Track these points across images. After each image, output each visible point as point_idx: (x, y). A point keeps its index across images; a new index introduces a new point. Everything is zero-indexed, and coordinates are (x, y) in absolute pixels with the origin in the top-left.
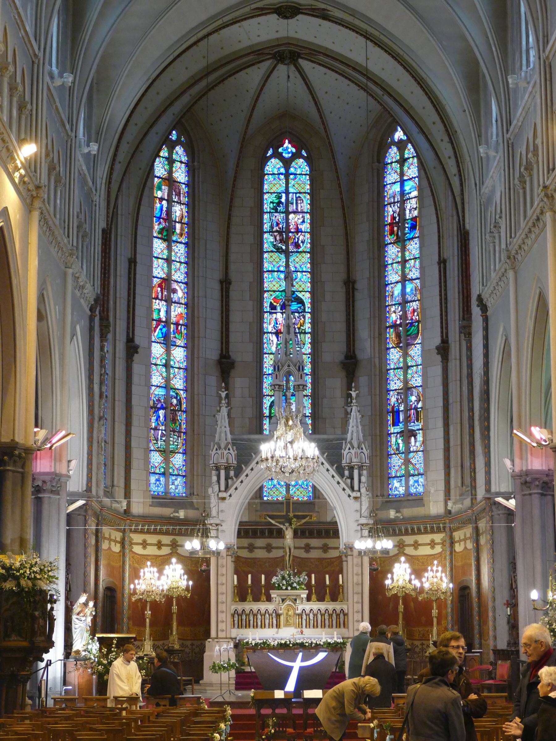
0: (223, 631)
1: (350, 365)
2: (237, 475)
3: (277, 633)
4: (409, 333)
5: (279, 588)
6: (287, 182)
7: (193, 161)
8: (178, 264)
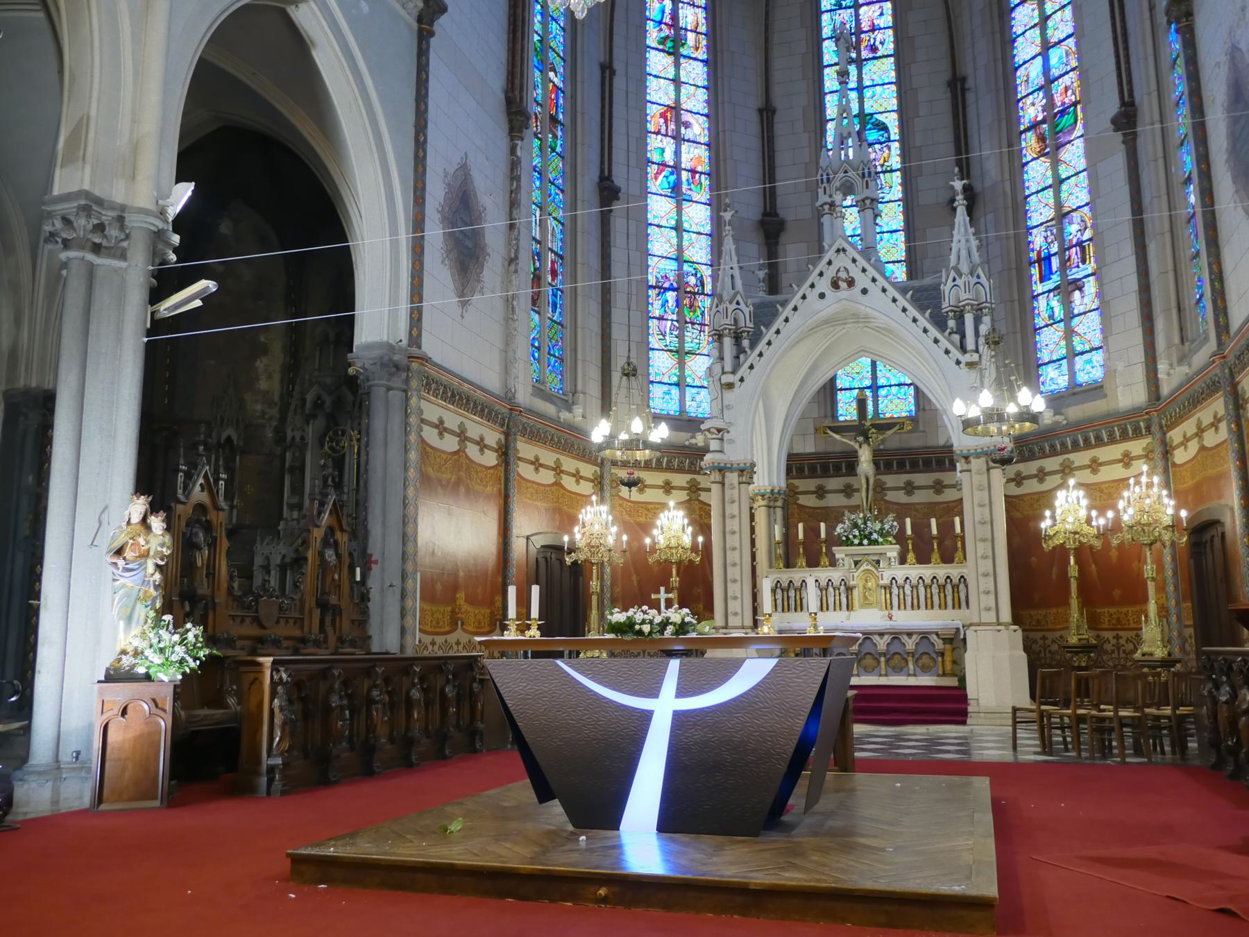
0: (736, 614)
2: (753, 346)
3: (848, 619)
5: (848, 543)
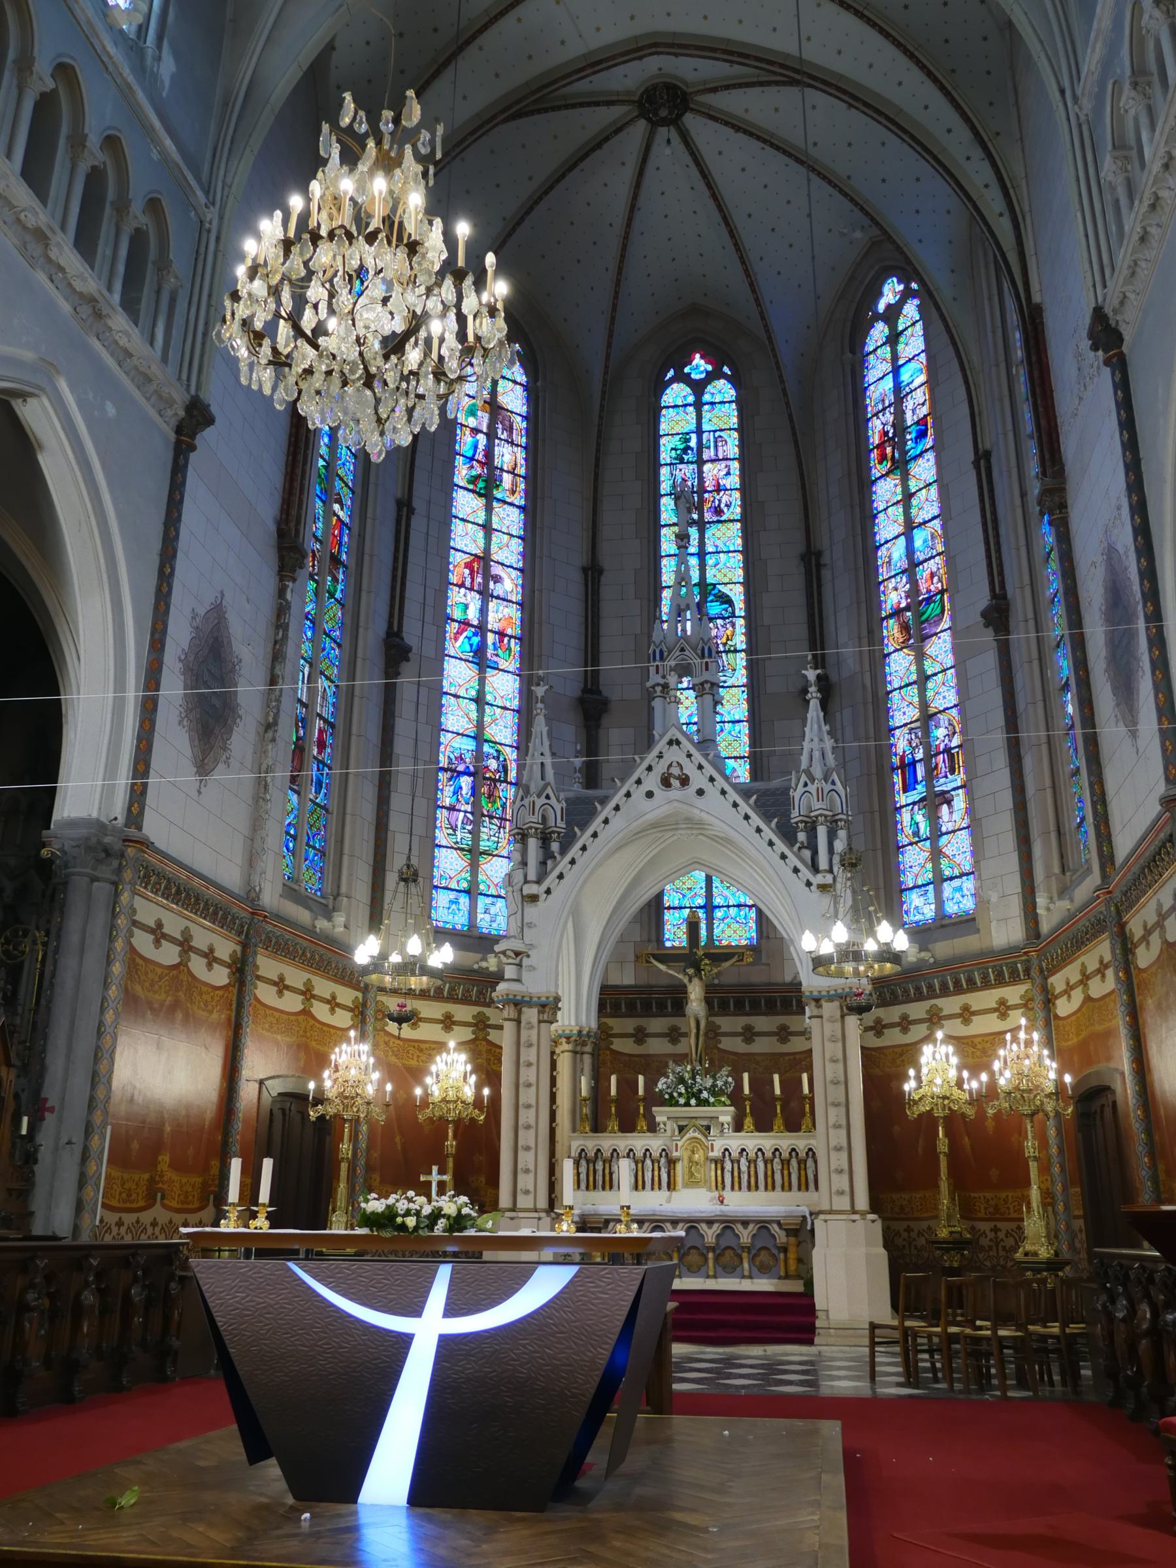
0: (527, 1192)
2: (564, 851)
3: (669, 1201)
4: (924, 618)
6: (700, 421)
7: (536, 380)
8: (506, 537)
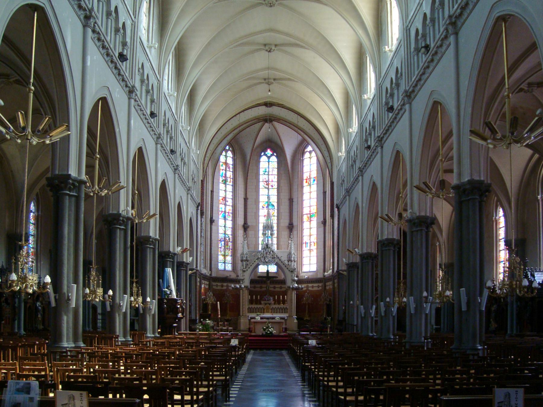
1: (291, 227)
6: (268, 165)
